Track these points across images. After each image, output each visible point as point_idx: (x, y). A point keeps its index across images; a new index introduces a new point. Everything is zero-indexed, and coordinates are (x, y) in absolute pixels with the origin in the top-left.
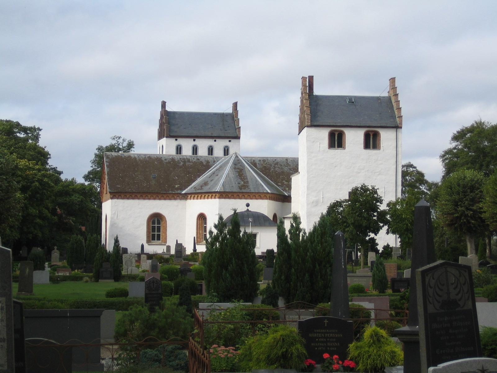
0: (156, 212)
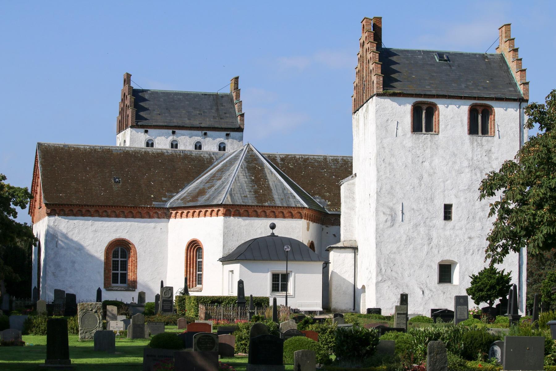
0: (121, 237)
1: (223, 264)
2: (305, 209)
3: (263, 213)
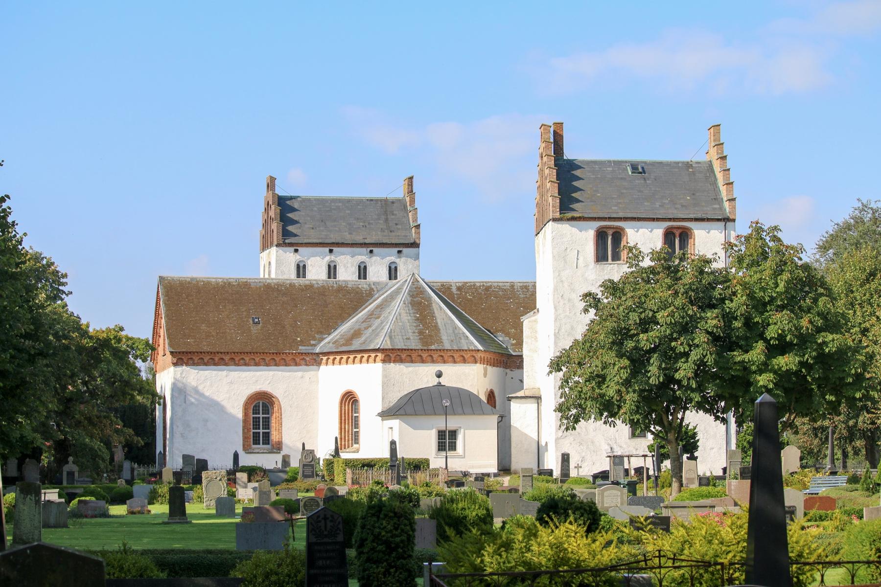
1: (382, 420)
2: (480, 352)
3: (429, 358)
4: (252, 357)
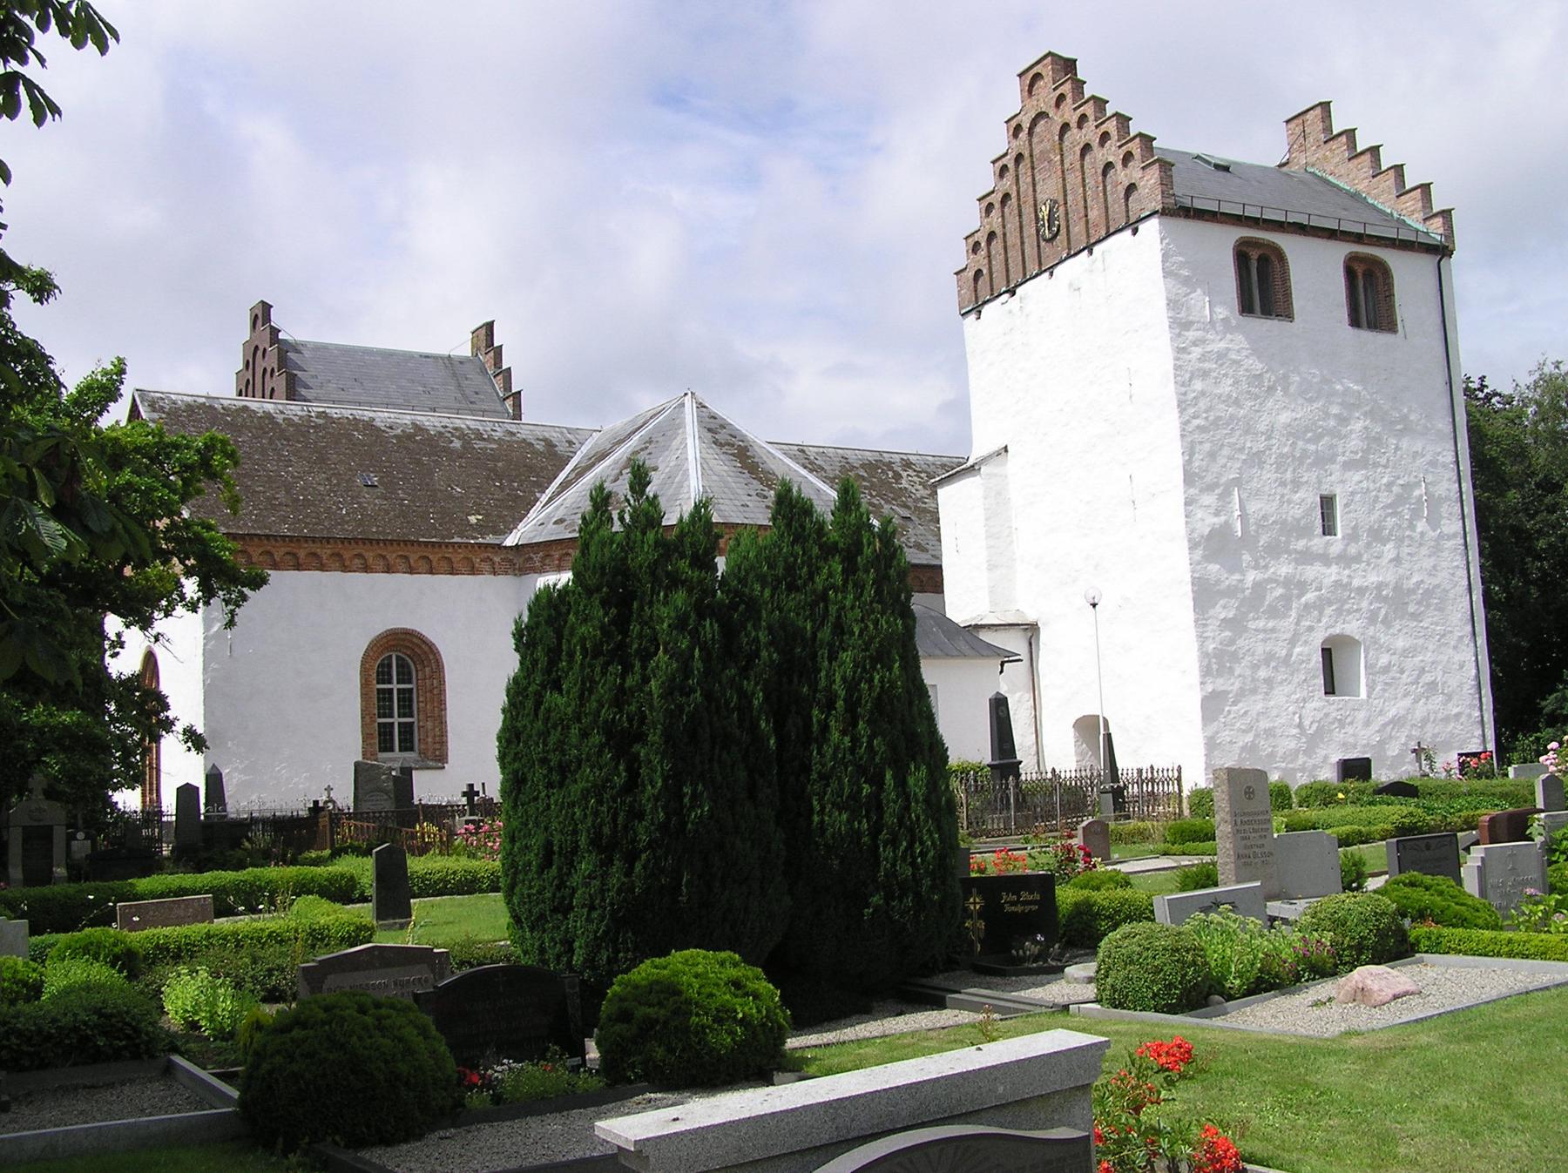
4: (379, 552)
